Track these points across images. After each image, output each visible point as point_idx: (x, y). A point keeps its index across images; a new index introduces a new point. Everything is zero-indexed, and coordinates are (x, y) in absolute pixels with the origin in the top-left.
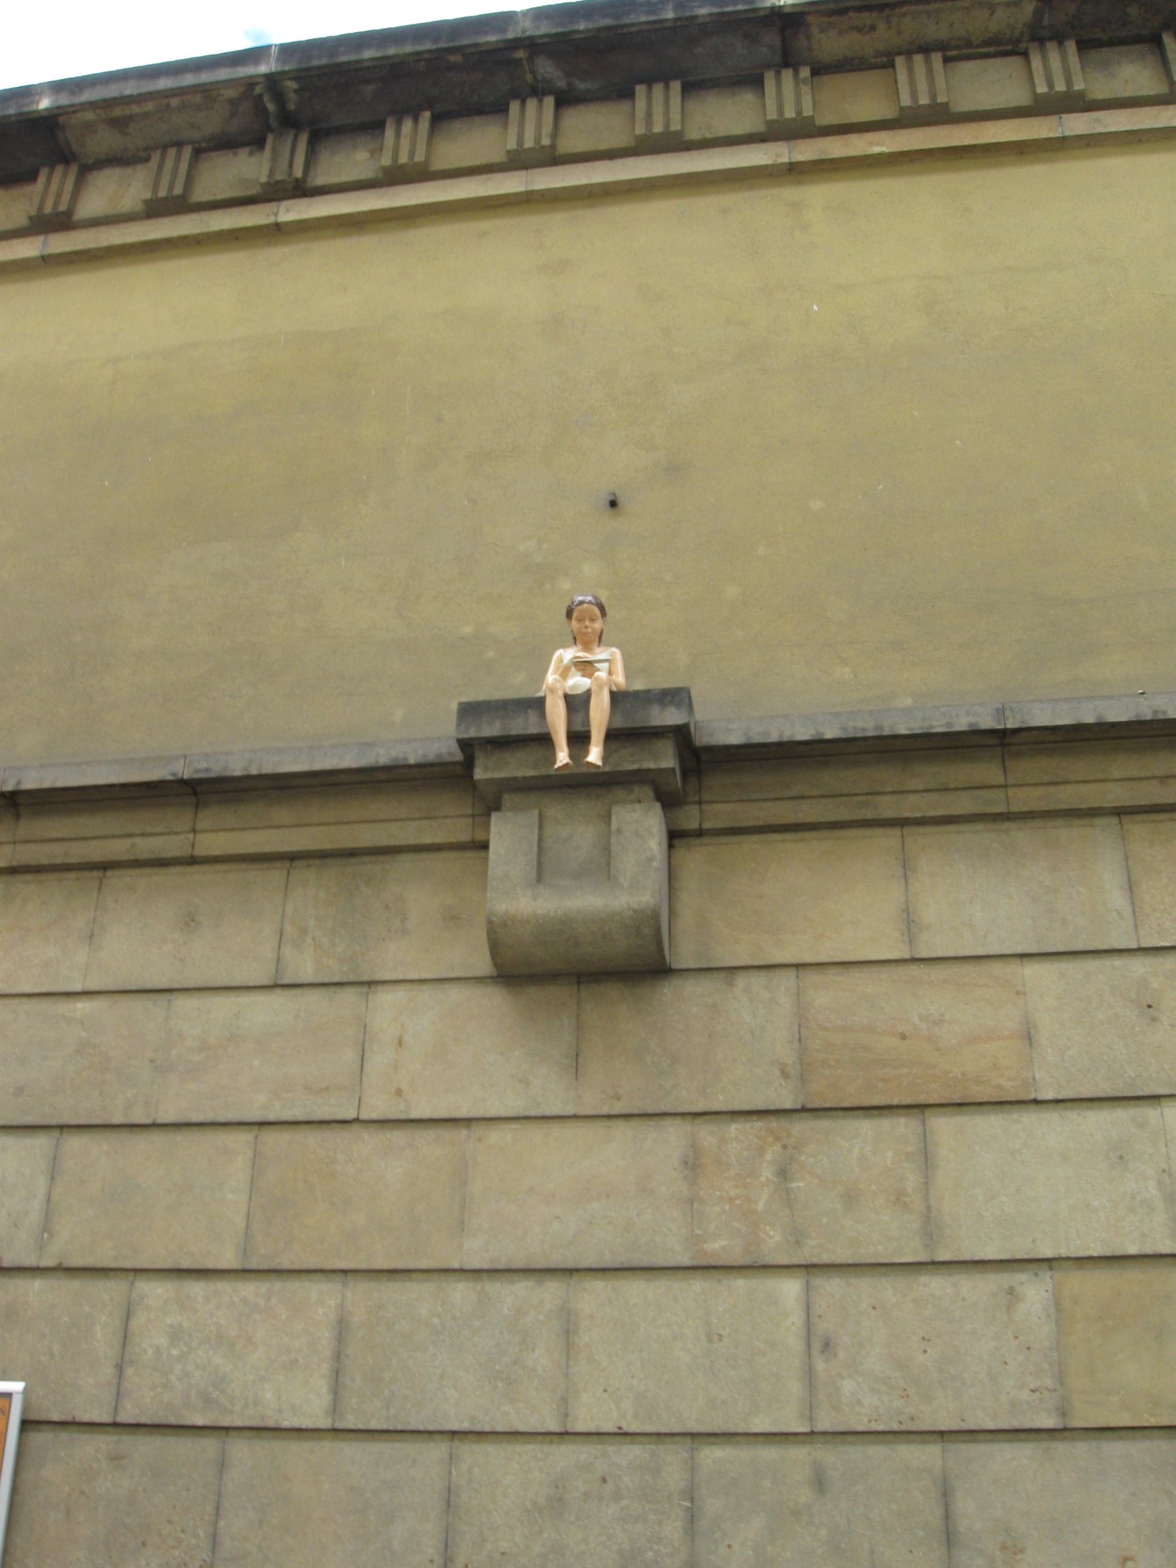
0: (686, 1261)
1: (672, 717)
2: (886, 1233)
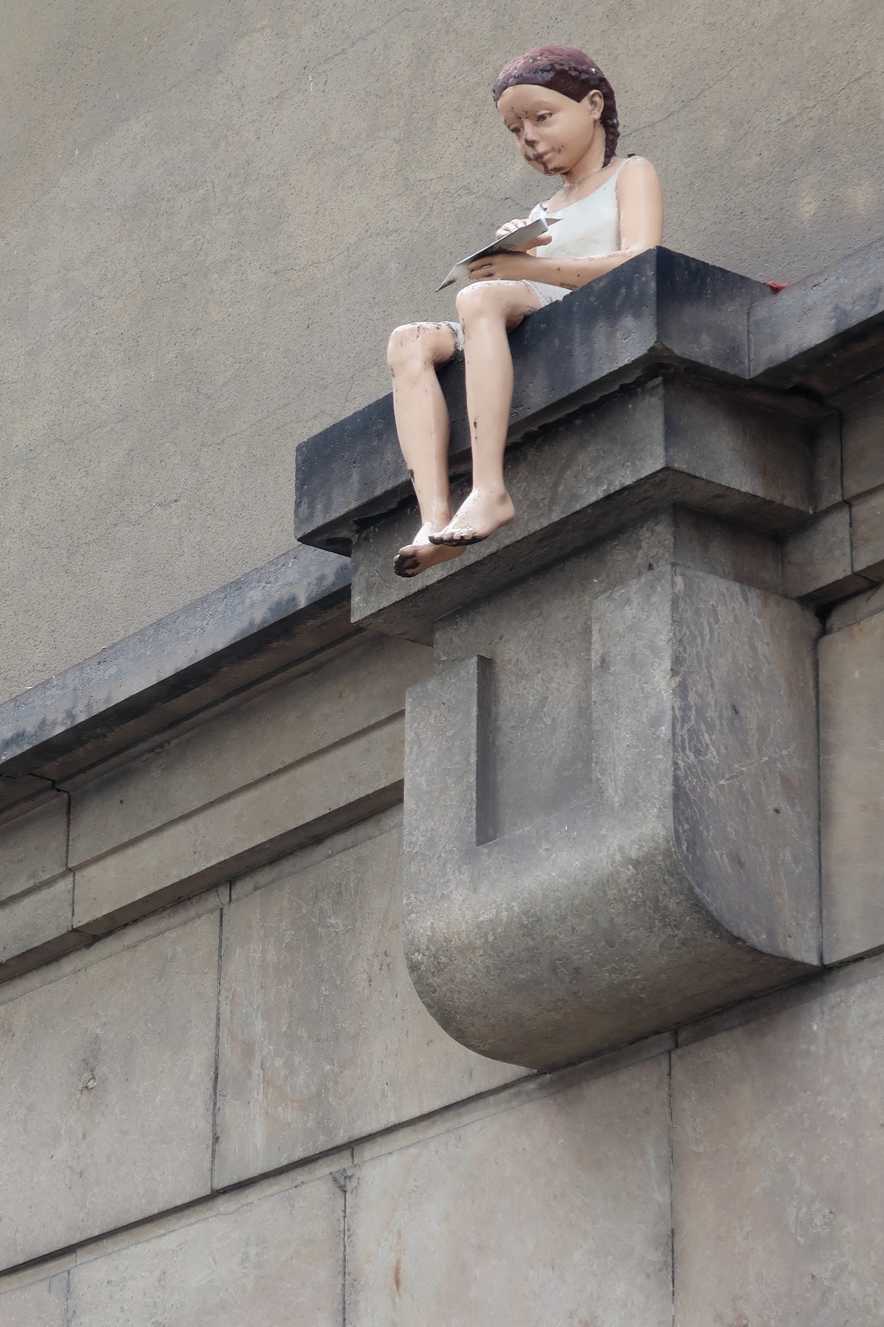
1: (627, 342)
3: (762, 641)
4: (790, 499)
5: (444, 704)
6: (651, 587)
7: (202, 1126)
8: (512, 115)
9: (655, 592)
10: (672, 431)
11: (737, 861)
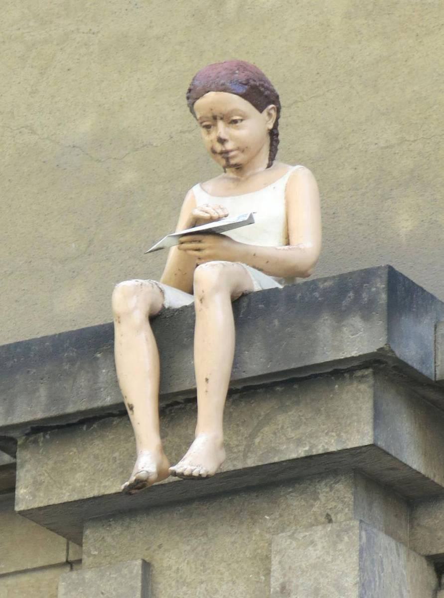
1: (357, 339)
3: (406, 589)
5: (102, 593)
6: (338, 536)
8: (210, 115)
9: (342, 541)
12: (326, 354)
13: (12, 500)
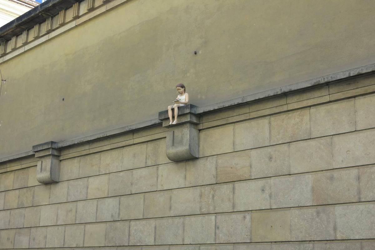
0: (199, 213)
1: (188, 111)
2: (227, 207)
4: (198, 123)
7: (145, 161)
10: (190, 118)
11: (193, 150)
12: (185, 112)
13: (162, 126)
